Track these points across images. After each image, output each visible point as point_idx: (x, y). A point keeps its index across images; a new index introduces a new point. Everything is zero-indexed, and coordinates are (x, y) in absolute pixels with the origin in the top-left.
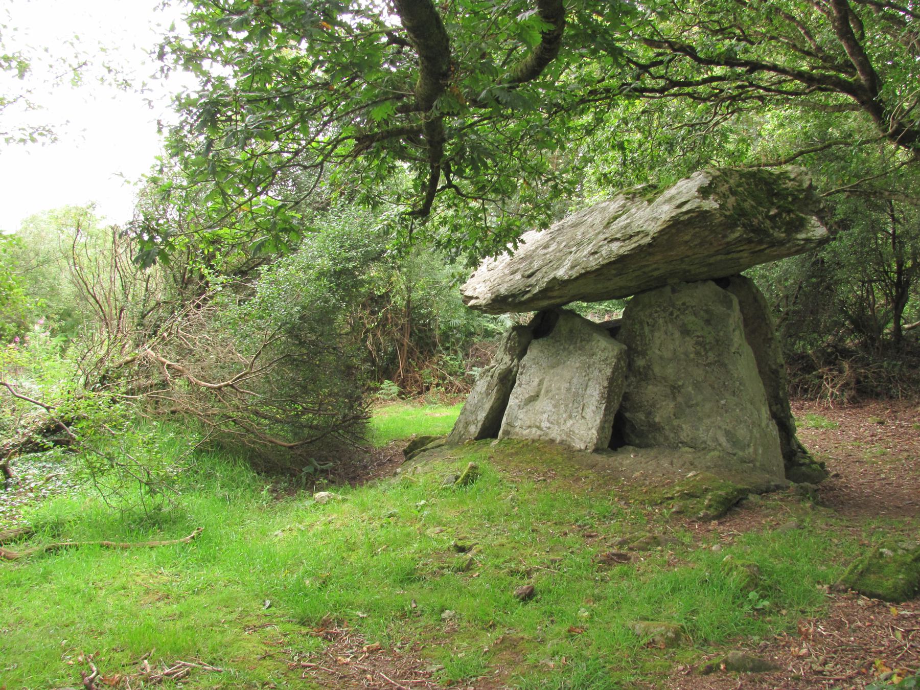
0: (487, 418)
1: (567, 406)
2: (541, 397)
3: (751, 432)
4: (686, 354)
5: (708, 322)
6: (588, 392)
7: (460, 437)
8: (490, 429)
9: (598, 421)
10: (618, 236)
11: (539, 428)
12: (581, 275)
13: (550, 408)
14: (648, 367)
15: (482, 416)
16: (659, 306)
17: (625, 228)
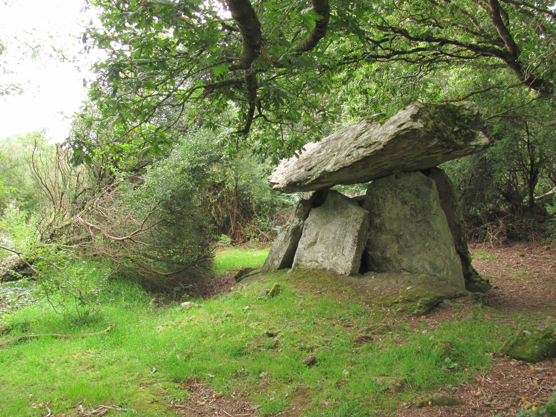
0: (285, 256)
1: (333, 248)
2: (317, 243)
3: (445, 262)
4: (405, 216)
5: (417, 196)
6: (346, 239)
7: (269, 268)
8: (287, 263)
9: (352, 257)
10: (363, 145)
11: (316, 261)
12: (341, 169)
13: (323, 249)
14: (382, 224)
15: (282, 255)
16: (388, 187)
17: (367, 140)
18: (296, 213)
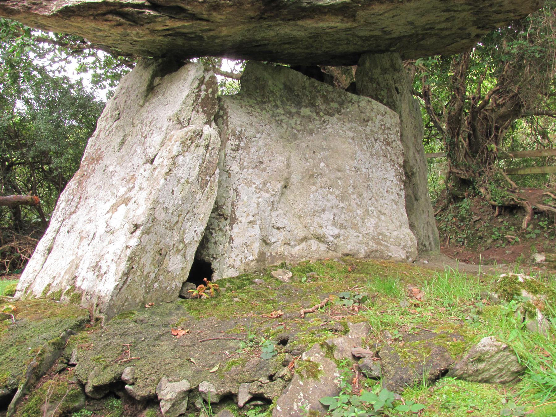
11: (320, 238)
18: (198, 96)
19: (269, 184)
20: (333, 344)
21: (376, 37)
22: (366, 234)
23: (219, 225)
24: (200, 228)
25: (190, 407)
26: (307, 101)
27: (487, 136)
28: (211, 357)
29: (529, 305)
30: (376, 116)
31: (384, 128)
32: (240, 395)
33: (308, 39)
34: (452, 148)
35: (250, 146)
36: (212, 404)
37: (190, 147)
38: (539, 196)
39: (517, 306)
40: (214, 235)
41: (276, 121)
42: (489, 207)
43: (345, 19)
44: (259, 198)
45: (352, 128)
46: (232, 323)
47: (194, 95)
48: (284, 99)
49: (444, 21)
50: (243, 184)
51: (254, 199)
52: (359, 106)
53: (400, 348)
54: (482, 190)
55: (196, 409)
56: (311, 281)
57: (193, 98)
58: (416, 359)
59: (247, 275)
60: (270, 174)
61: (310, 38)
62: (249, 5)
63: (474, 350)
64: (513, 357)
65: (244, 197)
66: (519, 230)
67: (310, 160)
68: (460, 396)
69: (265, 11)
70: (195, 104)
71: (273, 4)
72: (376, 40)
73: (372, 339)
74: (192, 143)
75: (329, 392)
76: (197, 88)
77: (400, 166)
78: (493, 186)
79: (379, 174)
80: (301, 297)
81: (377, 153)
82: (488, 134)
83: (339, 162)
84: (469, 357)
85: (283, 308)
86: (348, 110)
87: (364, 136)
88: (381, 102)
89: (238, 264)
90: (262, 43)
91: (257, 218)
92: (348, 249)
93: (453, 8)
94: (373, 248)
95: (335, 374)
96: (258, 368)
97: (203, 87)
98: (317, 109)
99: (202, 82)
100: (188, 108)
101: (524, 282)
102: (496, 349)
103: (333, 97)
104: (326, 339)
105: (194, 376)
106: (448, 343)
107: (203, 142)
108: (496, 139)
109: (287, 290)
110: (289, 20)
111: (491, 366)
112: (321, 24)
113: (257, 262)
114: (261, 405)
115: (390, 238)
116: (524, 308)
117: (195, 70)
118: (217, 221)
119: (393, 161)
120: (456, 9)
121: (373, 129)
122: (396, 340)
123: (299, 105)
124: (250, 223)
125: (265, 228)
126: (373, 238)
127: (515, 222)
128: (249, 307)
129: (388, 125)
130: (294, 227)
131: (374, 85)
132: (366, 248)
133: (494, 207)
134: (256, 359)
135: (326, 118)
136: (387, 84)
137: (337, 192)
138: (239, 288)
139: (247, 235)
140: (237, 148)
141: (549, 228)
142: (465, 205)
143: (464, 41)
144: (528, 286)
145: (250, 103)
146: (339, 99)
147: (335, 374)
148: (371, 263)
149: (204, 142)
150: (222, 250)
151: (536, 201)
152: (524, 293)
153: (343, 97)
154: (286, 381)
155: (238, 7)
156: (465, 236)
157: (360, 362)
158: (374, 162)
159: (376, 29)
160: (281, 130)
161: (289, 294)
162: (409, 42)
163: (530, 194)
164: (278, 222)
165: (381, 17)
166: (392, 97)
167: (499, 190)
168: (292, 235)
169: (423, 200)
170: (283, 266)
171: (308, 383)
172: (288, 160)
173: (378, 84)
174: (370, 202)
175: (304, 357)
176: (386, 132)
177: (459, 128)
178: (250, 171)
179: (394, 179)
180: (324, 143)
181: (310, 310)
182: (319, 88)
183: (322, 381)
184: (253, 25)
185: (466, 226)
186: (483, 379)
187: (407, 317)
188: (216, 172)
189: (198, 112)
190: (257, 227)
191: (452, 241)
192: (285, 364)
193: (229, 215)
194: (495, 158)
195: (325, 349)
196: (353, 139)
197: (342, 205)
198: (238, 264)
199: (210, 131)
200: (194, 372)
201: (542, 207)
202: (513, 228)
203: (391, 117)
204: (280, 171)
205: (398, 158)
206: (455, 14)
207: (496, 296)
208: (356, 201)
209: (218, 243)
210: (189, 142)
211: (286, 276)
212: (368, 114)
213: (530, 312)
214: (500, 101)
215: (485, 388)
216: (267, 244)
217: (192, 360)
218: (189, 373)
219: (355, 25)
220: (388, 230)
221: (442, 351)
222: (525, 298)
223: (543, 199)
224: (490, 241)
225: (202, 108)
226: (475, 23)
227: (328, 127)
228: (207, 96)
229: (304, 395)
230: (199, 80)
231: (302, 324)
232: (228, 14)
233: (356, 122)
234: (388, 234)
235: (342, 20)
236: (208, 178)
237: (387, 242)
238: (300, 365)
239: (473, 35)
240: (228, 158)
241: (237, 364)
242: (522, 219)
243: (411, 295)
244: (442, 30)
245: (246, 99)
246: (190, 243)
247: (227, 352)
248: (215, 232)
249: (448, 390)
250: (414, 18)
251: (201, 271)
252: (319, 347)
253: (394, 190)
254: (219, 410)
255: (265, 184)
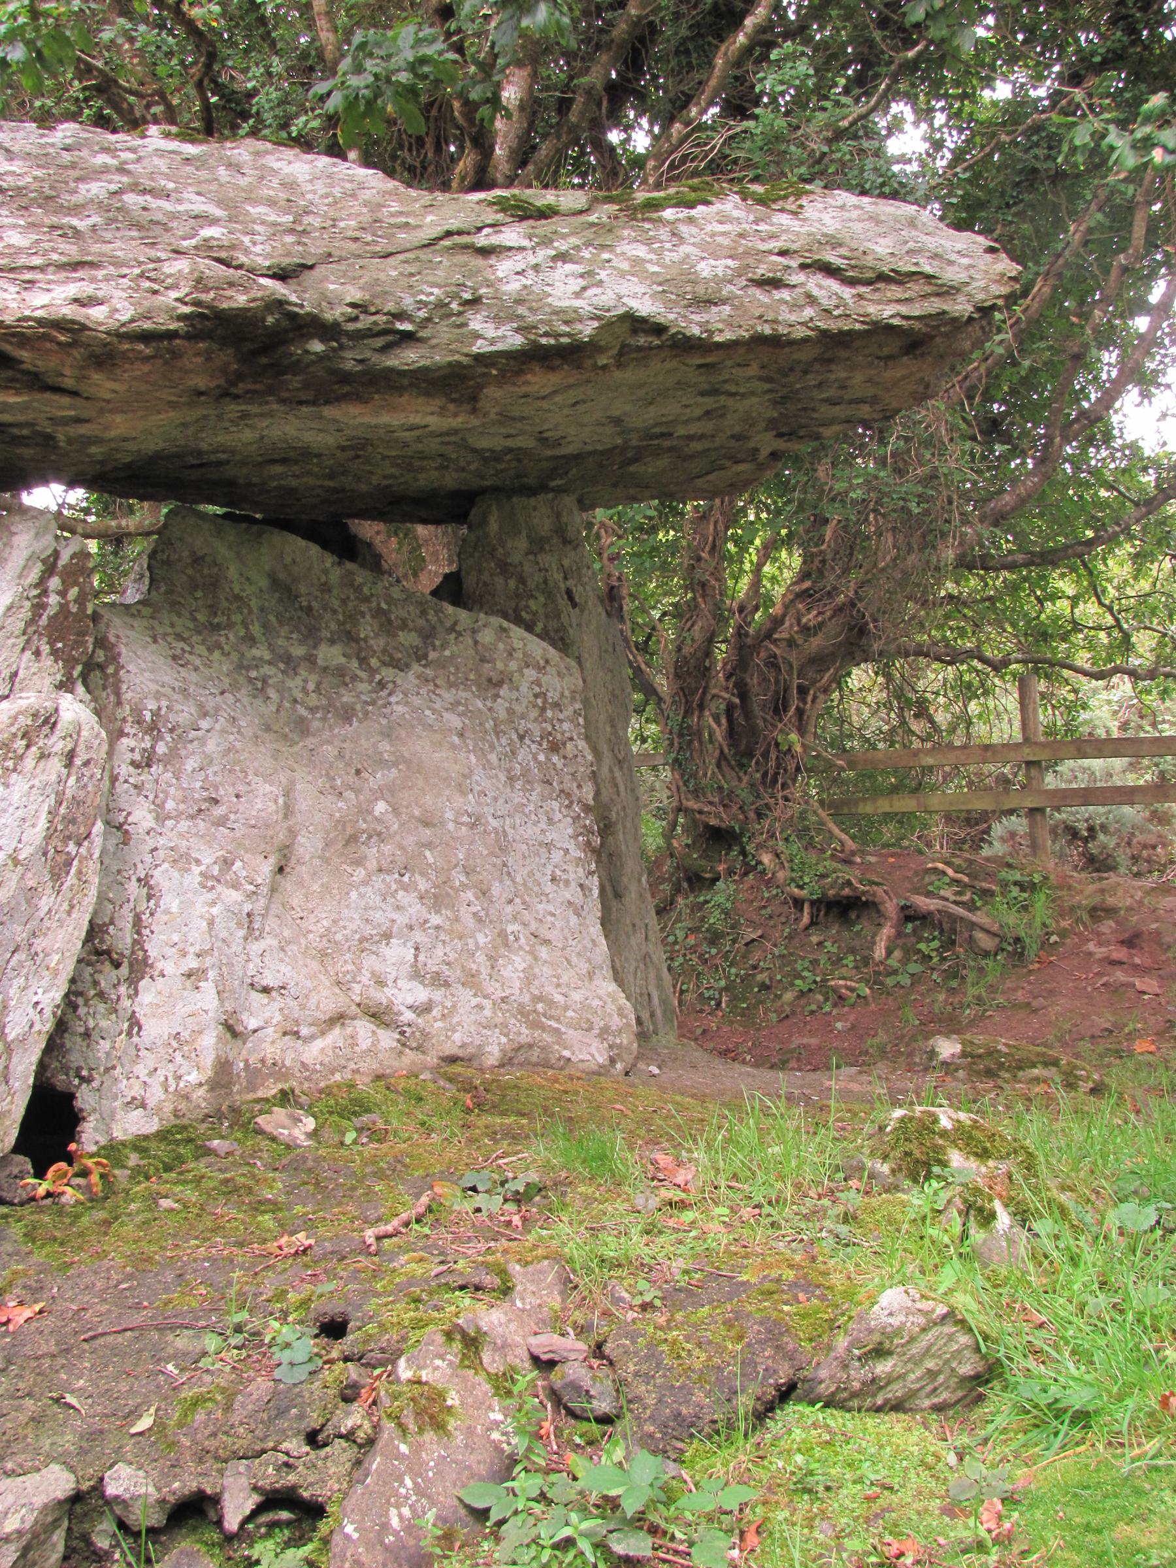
11: (379, 1016)
18: (39, 607)
19: (238, 864)
20: (478, 1330)
21: (518, 454)
22: (503, 1000)
23: (96, 983)
24: (52, 996)
25: (74, 1550)
26: (333, 626)
27: (776, 711)
28: (124, 1387)
29: (977, 1191)
30: (520, 670)
31: (543, 703)
32: (226, 1496)
33: (339, 453)
34: (683, 743)
35: (183, 753)
36: (151, 1531)
37: (21, 757)
38: (916, 873)
39: (944, 1196)
40: (82, 1011)
41: (251, 680)
42: (785, 903)
43: (451, 407)
44: (213, 903)
45: (458, 703)
46: (170, 1277)
47: (28, 604)
48: (272, 618)
49: (699, 419)
50: (166, 865)
51: (200, 908)
52: (476, 643)
53: (661, 1328)
54: (766, 859)
55: (94, 1553)
56: (371, 1140)
57: (25, 613)
58: (710, 1358)
59: (184, 1128)
60: (238, 834)
61: (343, 449)
62: (199, 360)
63: (863, 1326)
64: (964, 1339)
65: (170, 902)
66: (866, 965)
67: (349, 794)
68: (837, 1454)
69: (240, 377)
70: (30, 630)
71: (265, 361)
72: (519, 460)
73: (578, 1307)
74: (28, 746)
75: (483, 1469)
76: (36, 586)
77: (587, 809)
78: (796, 846)
79: (531, 831)
80: (353, 1189)
81: (526, 773)
82: (779, 707)
83: (428, 800)
84: (851, 1345)
85: (308, 1225)
86: (447, 653)
87: (489, 725)
88: (529, 628)
89: (155, 1095)
90: (213, 458)
91: (208, 961)
92: (454, 1042)
93: (727, 387)
94: (523, 1039)
95: (492, 1416)
96: (273, 1413)
97: (55, 583)
98: (360, 649)
99: (50, 569)
100: (11, 641)
101: (956, 1130)
102: (922, 1320)
103: (404, 614)
104: (457, 1315)
105: (82, 1452)
106: (786, 1308)
107: (57, 744)
108: (800, 719)
109: (310, 1170)
110: (301, 403)
111: (910, 1366)
112: (385, 419)
113: (212, 1089)
114: (289, 1523)
115: (566, 1008)
116: (965, 1201)
117: (32, 533)
118: (90, 969)
119: (568, 795)
120: (733, 389)
121: (516, 707)
122: (645, 1307)
123: (311, 635)
124: (189, 976)
125: (233, 991)
126: (522, 1012)
127: (856, 943)
128: (209, 1224)
129: (553, 696)
130: (309, 984)
131: (512, 584)
132: (504, 1040)
133: (798, 903)
134: (261, 1386)
135: (388, 673)
136: (545, 581)
137: (423, 885)
138: (168, 1168)
139: (182, 1010)
140: (147, 761)
141: (944, 959)
142: (720, 899)
143: (741, 467)
144: (965, 1138)
145: (178, 629)
146: (421, 622)
147: (492, 1416)
148: (524, 1084)
149: (61, 744)
150: (108, 1054)
151: (907, 885)
152: (956, 1158)
153: (431, 615)
154: (361, 1446)
155: (166, 363)
156: (723, 983)
157: (556, 1377)
158: (518, 798)
159: (522, 433)
160: (263, 709)
161: (317, 1184)
162: (601, 466)
163: (892, 865)
164: (266, 972)
165: (545, 404)
166: (558, 616)
167: (812, 857)
168: (303, 1007)
169: (633, 895)
170: (285, 1098)
171: (421, 1446)
172: (286, 795)
173: (522, 580)
174: (509, 909)
175: (405, 1371)
176: (549, 714)
177: (706, 689)
178: (184, 825)
179: (571, 845)
180: (385, 746)
181: (389, 1228)
182: (366, 590)
183: (459, 1439)
184: (198, 412)
185: (726, 956)
186: (887, 1401)
187: (661, 1239)
188: (95, 831)
189: (37, 653)
190: (208, 987)
191: (688, 997)
192: (349, 1394)
193: (127, 953)
194: (798, 769)
195: (457, 1345)
196: (461, 735)
197: (436, 920)
198: (155, 1095)
199: (74, 709)
200: (81, 1437)
201: (924, 903)
202: (850, 960)
203: (559, 674)
204: (267, 826)
205: (579, 787)
206: (730, 402)
207: (885, 1169)
208: (473, 909)
209: (95, 1036)
210: (20, 744)
211: (298, 1129)
212: (500, 665)
213: (980, 1210)
214: (810, 618)
215: (898, 1428)
216: (235, 1034)
217: (70, 1399)
218: (68, 1441)
219: (475, 422)
220: (558, 985)
221: (775, 1332)
222: (960, 1171)
223: (927, 879)
224: (789, 996)
225: (51, 643)
226: (772, 424)
227: (393, 699)
228: (63, 607)
229: (416, 1484)
230: (44, 561)
231: (376, 1274)
232: (135, 378)
233: (467, 688)
234: (558, 998)
235: (443, 408)
236: (72, 848)
237: (558, 1020)
238: (395, 1397)
239: (764, 453)
240: (121, 787)
241: (209, 1404)
242: (874, 935)
243: (657, 1178)
244: (690, 438)
245: (165, 616)
246: (22, 1040)
247: (170, 1367)
248: (86, 1004)
249: (804, 1441)
250: (628, 408)
251: (51, 1124)
252: (440, 1339)
253: (572, 876)
254: (166, 1550)
255: (227, 863)
